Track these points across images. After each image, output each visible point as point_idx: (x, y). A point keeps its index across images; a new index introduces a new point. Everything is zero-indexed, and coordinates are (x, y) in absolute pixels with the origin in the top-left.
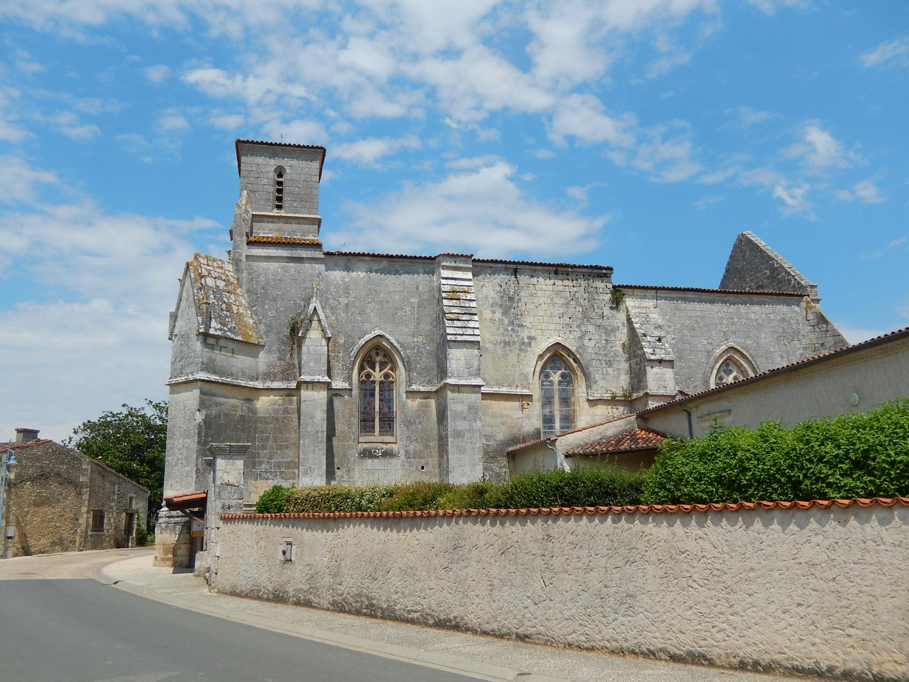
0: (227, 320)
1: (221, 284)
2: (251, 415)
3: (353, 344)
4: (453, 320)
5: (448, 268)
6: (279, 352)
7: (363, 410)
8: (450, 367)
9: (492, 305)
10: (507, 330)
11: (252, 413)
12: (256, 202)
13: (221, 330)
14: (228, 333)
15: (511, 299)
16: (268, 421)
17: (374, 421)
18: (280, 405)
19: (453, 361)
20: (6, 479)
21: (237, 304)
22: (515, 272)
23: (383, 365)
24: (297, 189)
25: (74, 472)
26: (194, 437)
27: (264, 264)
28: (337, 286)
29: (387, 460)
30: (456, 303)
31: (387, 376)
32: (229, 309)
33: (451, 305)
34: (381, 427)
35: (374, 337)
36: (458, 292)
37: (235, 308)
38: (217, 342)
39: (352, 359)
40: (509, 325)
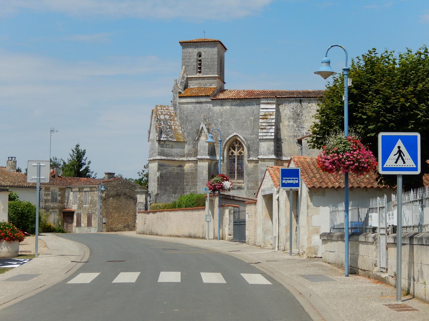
0: (169, 133)
1: (167, 117)
2: (181, 172)
3: (224, 140)
4: (262, 129)
5: (264, 103)
6: (193, 144)
7: (230, 169)
8: (260, 150)
9: (289, 118)
10: (295, 130)
11: (182, 171)
12: (189, 71)
13: (166, 138)
14: (169, 139)
15: (298, 115)
16: (189, 174)
17: (235, 173)
18: (193, 167)
19: (262, 148)
20: (101, 197)
21: (175, 125)
22: (301, 101)
23: (239, 148)
24: (207, 63)
25: (132, 193)
26: (156, 182)
27: (186, 106)
28: (217, 113)
29: (239, 190)
30: (265, 121)
31: (240, 153)
32: (170, 127)
33: (263, 122)
34: (238, 176)
35: (233, 136)
36: (267, 115)
37: (173, 127)
38: (165, 143)
39: (224, 146)
40: (296, 128)
